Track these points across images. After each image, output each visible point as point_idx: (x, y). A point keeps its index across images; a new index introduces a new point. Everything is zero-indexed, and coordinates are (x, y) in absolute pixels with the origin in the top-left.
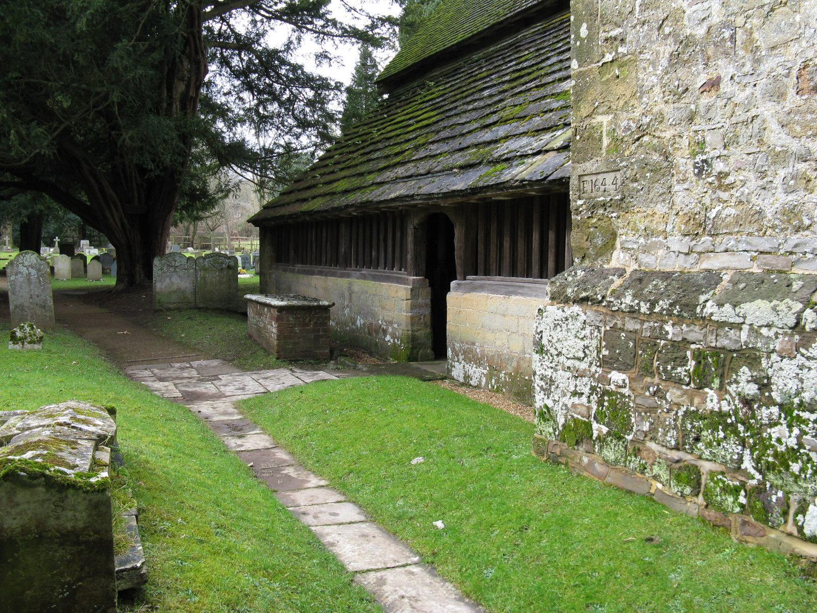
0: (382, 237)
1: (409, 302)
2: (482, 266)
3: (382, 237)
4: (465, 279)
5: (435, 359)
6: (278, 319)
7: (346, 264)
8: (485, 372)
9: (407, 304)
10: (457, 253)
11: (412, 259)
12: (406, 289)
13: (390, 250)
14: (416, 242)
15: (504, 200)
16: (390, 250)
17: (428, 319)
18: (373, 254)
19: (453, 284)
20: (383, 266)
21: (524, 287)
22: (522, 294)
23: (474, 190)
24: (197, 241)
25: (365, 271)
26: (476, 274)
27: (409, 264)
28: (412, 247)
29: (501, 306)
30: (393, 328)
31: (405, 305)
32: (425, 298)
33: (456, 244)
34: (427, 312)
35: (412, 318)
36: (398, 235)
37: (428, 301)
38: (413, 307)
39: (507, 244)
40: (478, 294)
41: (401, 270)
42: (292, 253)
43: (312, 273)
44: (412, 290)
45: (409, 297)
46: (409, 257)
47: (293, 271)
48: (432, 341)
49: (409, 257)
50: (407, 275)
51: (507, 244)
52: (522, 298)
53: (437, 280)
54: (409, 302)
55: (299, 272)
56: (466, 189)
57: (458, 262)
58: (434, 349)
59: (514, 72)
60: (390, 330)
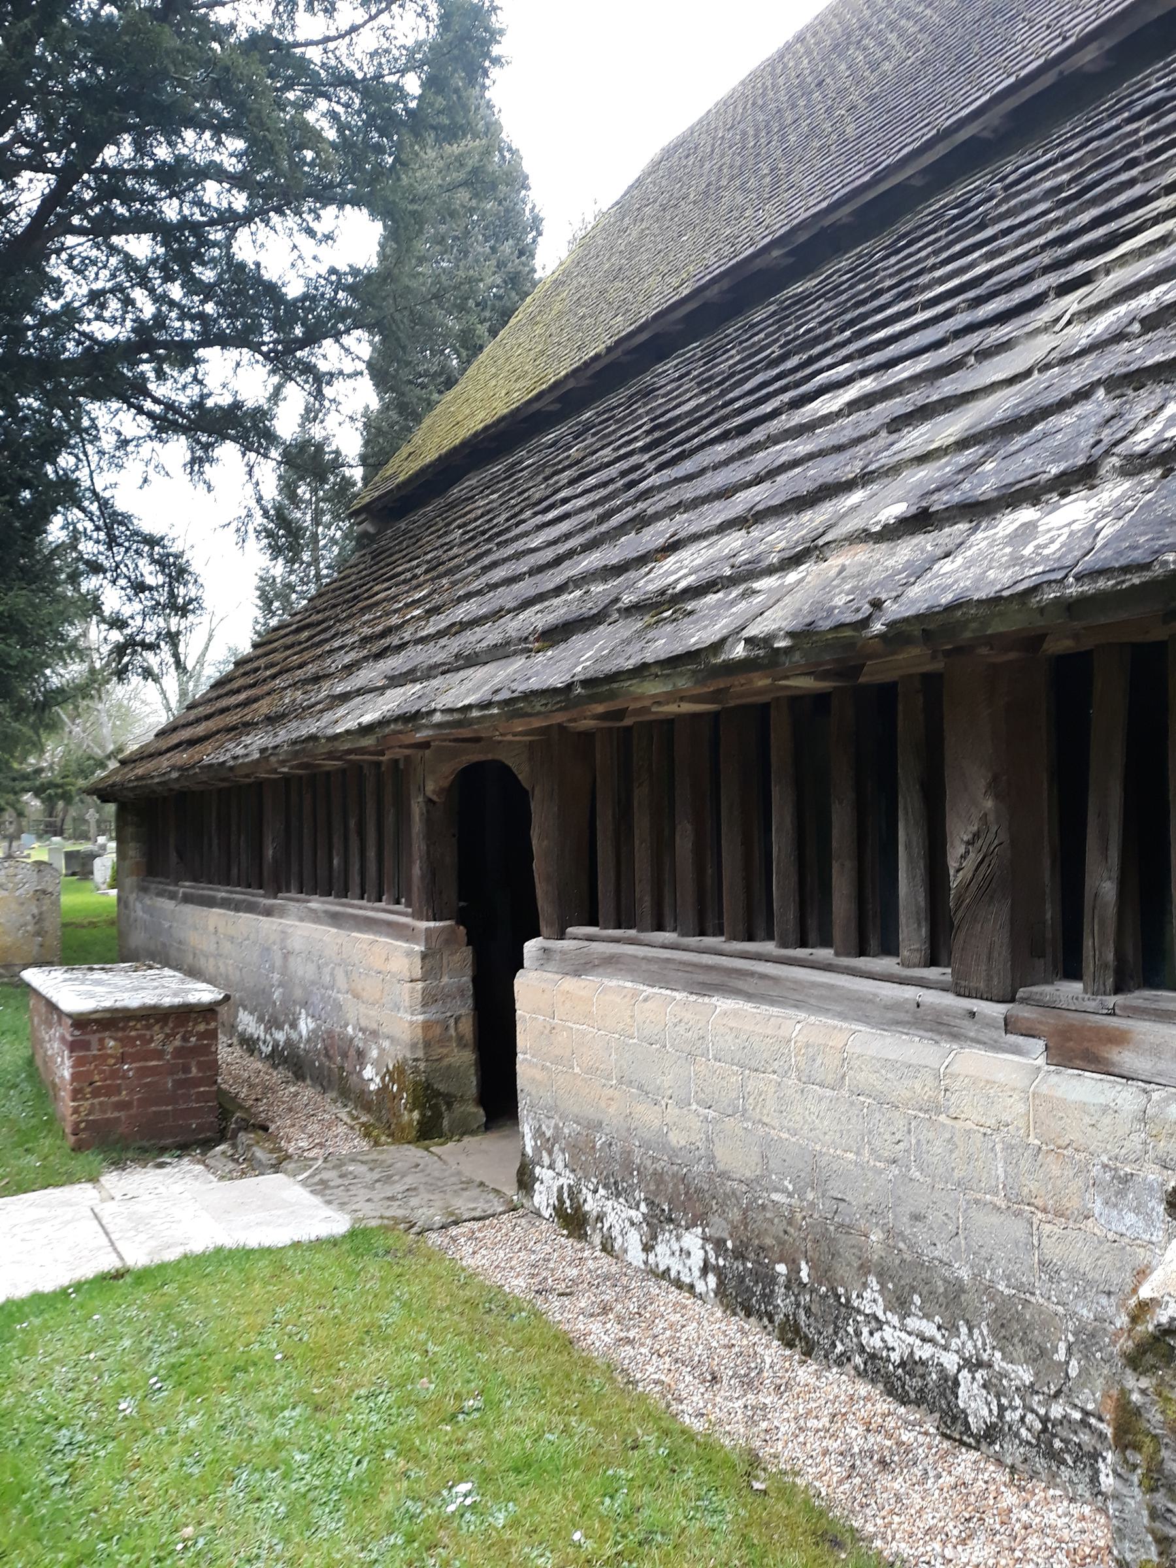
0: (352, 823)
1: (420, 986)
2: (598, 902)
3: (352, 823)
4: (561, 936)
5: (488, 1126)
6: (73, 1046)
7: (277, 886)
8: (636, 1216)
9: (413, 990)
10: (539, 867)
11: (423, 877)
12: (409, 954)
13: (371, 854)
14: (430, 835)
15: (695, 716)
16: (371, 854)
17: (467, 1027)
18: (335, 862)
19: (531, 947)
20: (358, 891)
21: (752, 974)
22: (749, 997)
23: (597, 685)
24: (69, 826)
25: (317, 904)
26: (593, 922)
27: (415, 889)
28: (424, 847)
29: (681, 1029)
30: (382, 1050)
31: (408, 994)
32: (458, 974)
33: (534, 842)
34: (464, 1008)
35: (427, 1026)
36: (390, 819)
37: (466, 979)
38: (429, 999)
39: (684, 843)
40: (606, 981)
41: (398, 903)
42: (174, 857)
43: (210, 903)
44: (424, 956)
45: (418, 973)
46: (416, 871)
47: (172, 896)
48: (475, 1082)
49: (416, 871)
50: (413, 916)
51: (684, 843)
52: (749, 1007)
53: (489, 933)
54: (420, 986)
55: (188, 899)
56: (569, 687)
57: (542, 890)
58: (484, 1100)
59: (648, 433)
60: (374, 1053)
